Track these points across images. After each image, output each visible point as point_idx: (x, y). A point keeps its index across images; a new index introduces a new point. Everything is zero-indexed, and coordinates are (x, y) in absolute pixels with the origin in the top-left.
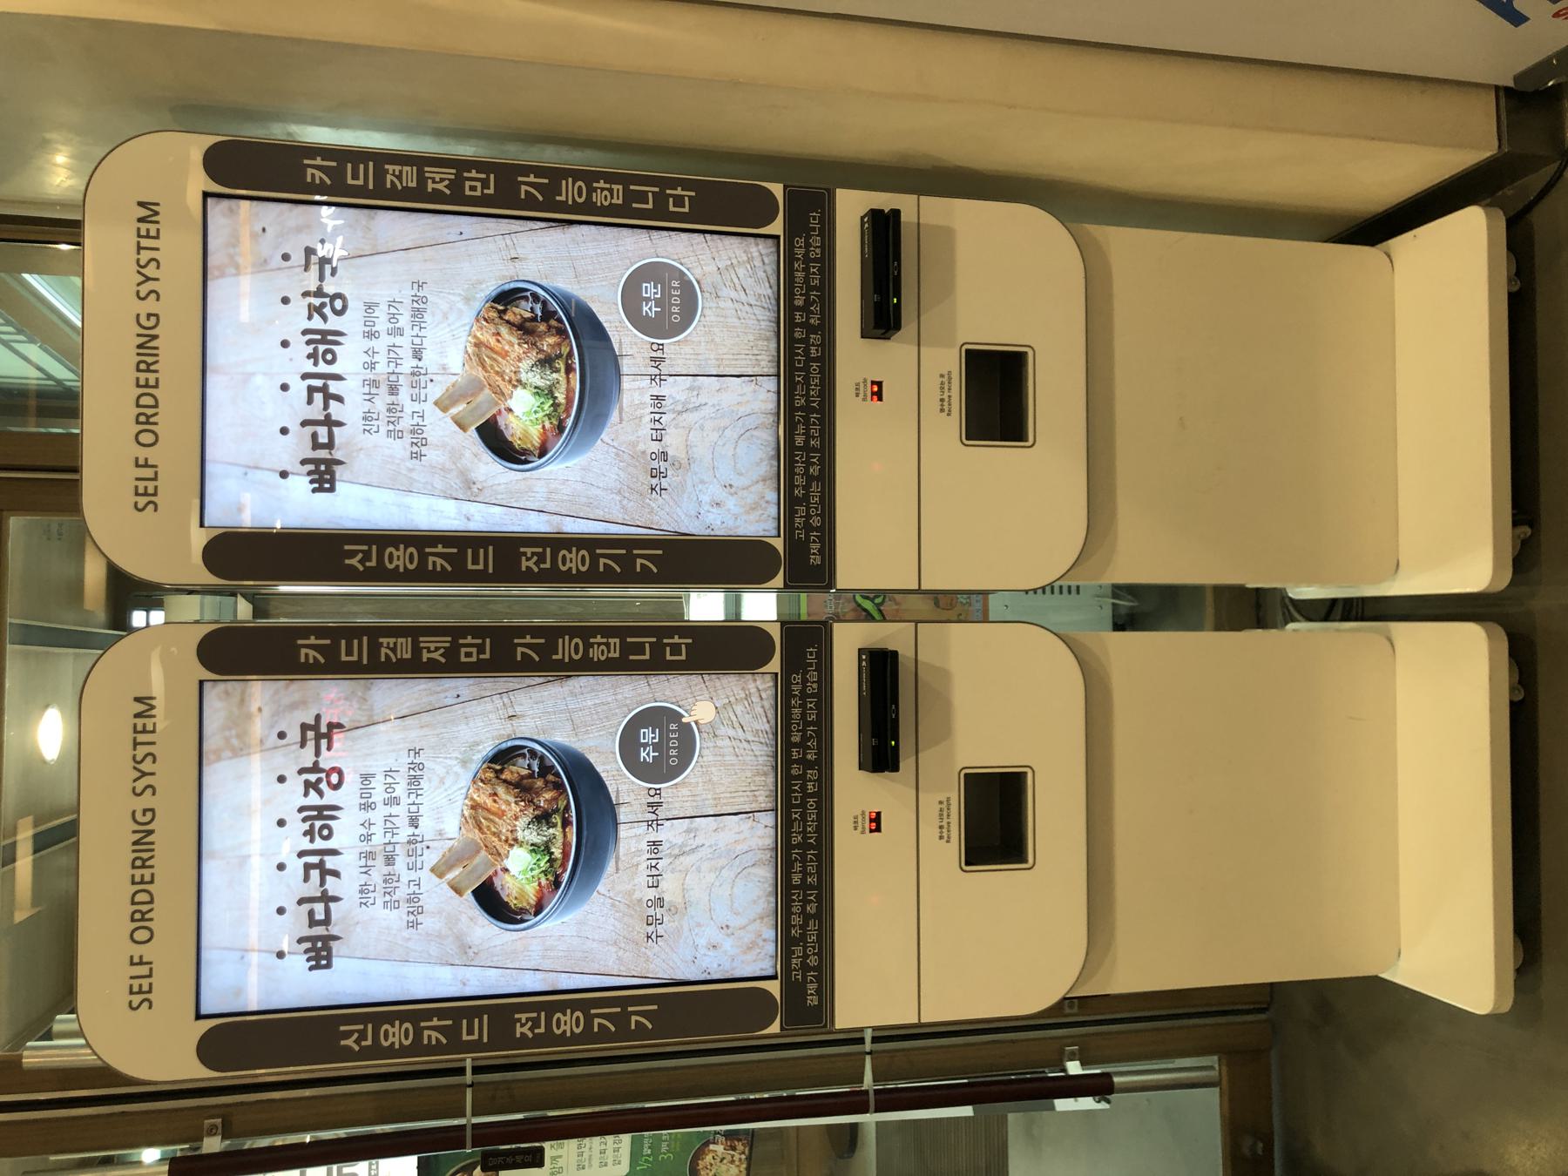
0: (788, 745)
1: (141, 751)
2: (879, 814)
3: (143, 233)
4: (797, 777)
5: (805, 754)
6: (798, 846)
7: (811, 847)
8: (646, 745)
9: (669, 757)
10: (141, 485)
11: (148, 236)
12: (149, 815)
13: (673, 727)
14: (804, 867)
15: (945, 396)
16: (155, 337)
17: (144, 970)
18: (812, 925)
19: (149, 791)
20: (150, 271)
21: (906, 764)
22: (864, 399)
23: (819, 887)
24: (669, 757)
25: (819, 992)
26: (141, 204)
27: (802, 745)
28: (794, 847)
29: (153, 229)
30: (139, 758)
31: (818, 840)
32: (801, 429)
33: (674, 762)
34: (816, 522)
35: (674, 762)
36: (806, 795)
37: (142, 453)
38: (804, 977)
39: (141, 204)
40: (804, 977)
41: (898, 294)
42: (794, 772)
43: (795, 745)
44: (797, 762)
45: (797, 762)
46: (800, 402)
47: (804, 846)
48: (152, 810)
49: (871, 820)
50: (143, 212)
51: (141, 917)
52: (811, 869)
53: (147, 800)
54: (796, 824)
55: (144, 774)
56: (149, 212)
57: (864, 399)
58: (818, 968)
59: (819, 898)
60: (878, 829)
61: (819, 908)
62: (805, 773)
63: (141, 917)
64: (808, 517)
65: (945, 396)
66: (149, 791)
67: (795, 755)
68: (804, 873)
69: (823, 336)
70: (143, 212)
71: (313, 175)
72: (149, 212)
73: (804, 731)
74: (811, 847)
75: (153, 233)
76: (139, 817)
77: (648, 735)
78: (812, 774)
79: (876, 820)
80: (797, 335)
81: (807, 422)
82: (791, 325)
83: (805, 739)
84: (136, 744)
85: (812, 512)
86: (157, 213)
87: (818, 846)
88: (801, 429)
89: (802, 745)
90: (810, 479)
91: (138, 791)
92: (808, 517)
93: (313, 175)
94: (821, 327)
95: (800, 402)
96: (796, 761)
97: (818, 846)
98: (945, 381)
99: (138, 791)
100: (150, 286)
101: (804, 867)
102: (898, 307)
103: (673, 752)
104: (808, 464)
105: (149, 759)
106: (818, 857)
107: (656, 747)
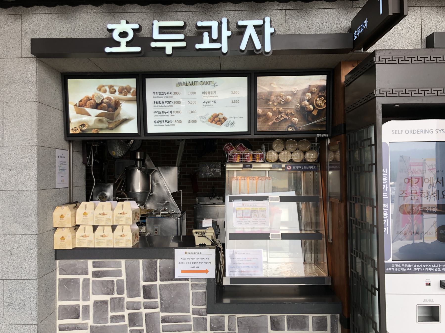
4: (438, 266)
6: (423, 266)
7: (422, 269)
10: (397, 131)
17: (400, 132)
18: (404, 269)
20: (442, 132)
23: (413, 271)
25: (389, 271)
31: (424, 271)
32: (418, 266)
34: (396, 269)
36: (434, 268)
37: (404, 131)
38: (393, 267)
40: (393, 267)
44: (442, 266)
45: (442, 266)
46: (424, 266)
47: (423, 268)
51: (411, 132)
52: (418, 269)
58: (395, 271)
59: (410, 271)
61: (408, 271)
63: (411, 132)
64: (397, 268)
68: (417, 268)
74: (422, 269)
78: (439, 269)
79: (429, 284)
81: (419, 267)
85: (399, 269)
87: (422, 271)
88: (418, 266)
90: (406, 268)
92: (397, 268)
94: (442, 271)
97: (422, 271)
98: (431, 301)
100: (439, 132)
104: (410, 268)
106: (420, 271)
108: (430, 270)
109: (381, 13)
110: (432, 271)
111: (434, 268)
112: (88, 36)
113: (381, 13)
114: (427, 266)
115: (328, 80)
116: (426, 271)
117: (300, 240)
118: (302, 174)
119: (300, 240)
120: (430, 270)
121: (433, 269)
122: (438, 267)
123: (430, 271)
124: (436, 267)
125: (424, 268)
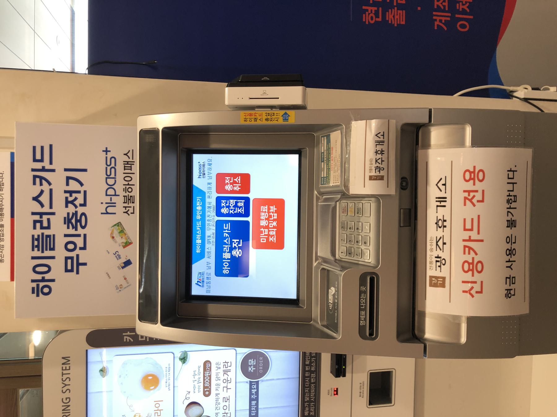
0: (304, 365)
1: (65, 377)
2: (337, 389)
3: (64, 368)
4: (308, 377)
5: (311, 368)
6: (308, 402)
7: (312, 402)
8: (251, 365)
9: (259, 369)
11: (66, 370)
12: (68, 400)
13: (261, 358)
14: (310, 409)
15: (362, 391)
16: (69, 406)
19: (68, 391)
20: (67, 382)
21: (348, 374)
22: (331, 396)
24: (259, 369)
26: (63, 358)
27: (310, 365)
28: (306, 402)
29: (68, 366)
30: (64, 380)
31: (315, 399)
32: (307, 409)
33: (261, 371)
35: (261, 371)
36: (311, 383)
39: (63, 358)
41: (345, 365)
42: (306, 375)
43: (307, 365)
44: (308, 371)
45: (308, 371)
46: (307, 399)
47: (310, 401)
48: (69, 398)
49: (335, 391)
50: (64, 361)
53: (67, 395)
54: (307, 394)
55: (66, 385)
56: (66, 360)
57: (331, 396)
60: (337, 394)
62: (310, 375)
65: (362, 391)
66: (68, 391)
67: (307, 369)
68: (310, 411)
69: (316, 374)
70: (64, 361)
71: (126, 339)
72: (66, 360)
73: (310, 360)
74: (312, 402)
75: (68, 368)
76: (65, 401)
77: (252, 362)
78: (313, 375)
80: (306, 375)
82: (304, 371)
83: (311, 363)
84: (63, 374)
86: (69, 361)
88: (307, 409)
89: (310, 365)
91: (64, 391)
93: (126, 339)
94: (315, 371)
95: (307, 399)
96: (307, 371)
97: (315, 402)
99: (64, 391)
101: (310, 409)
102: (345, 369)
103: (261, 368)
105: (68, 379)
107: (254, 366)
108: (313, 391)
109: (446, 29)
110: (315, 387)
111: (311, 383)
112: (496, 359)
113: (446, 29)
114: (307, 395)
115: (38, 329)
116: (315, 395)
117: (414, 359)
118: (447, 159)
119: (414, 359)
120: (313, 391)
121: (313, 385)
122: (310, 377)
123: (315, 390)
124: (310, 380)
125: (310, 399)
